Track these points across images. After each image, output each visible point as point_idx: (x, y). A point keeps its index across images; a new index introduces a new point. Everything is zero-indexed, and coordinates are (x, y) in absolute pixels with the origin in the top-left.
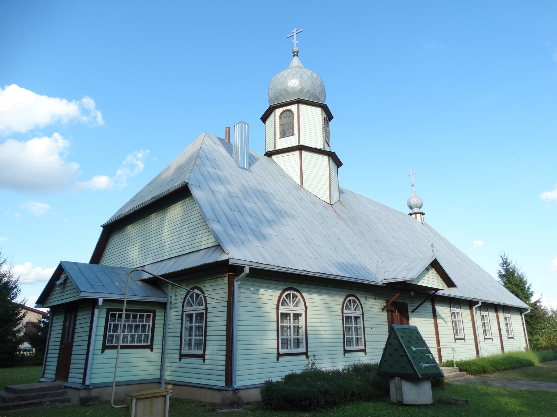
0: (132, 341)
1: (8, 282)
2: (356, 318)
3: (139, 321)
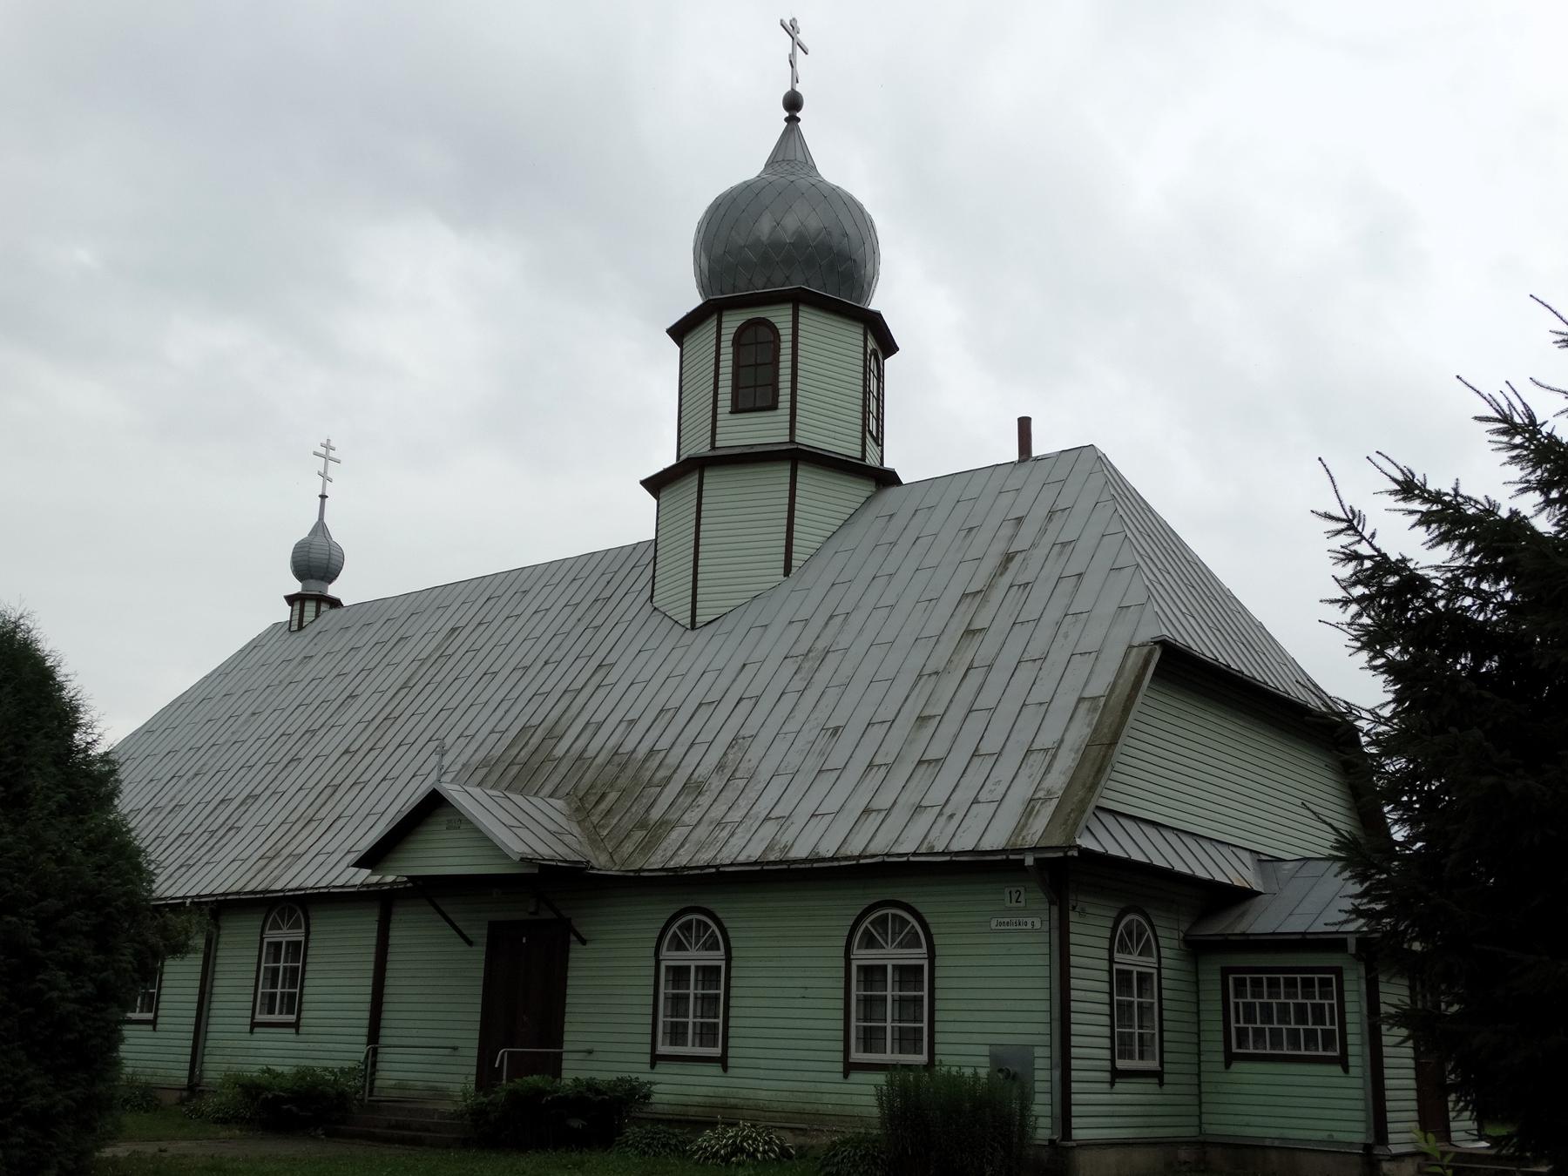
0: (1276, 1043)
2: (1144, 978)
3: (1270, 997)
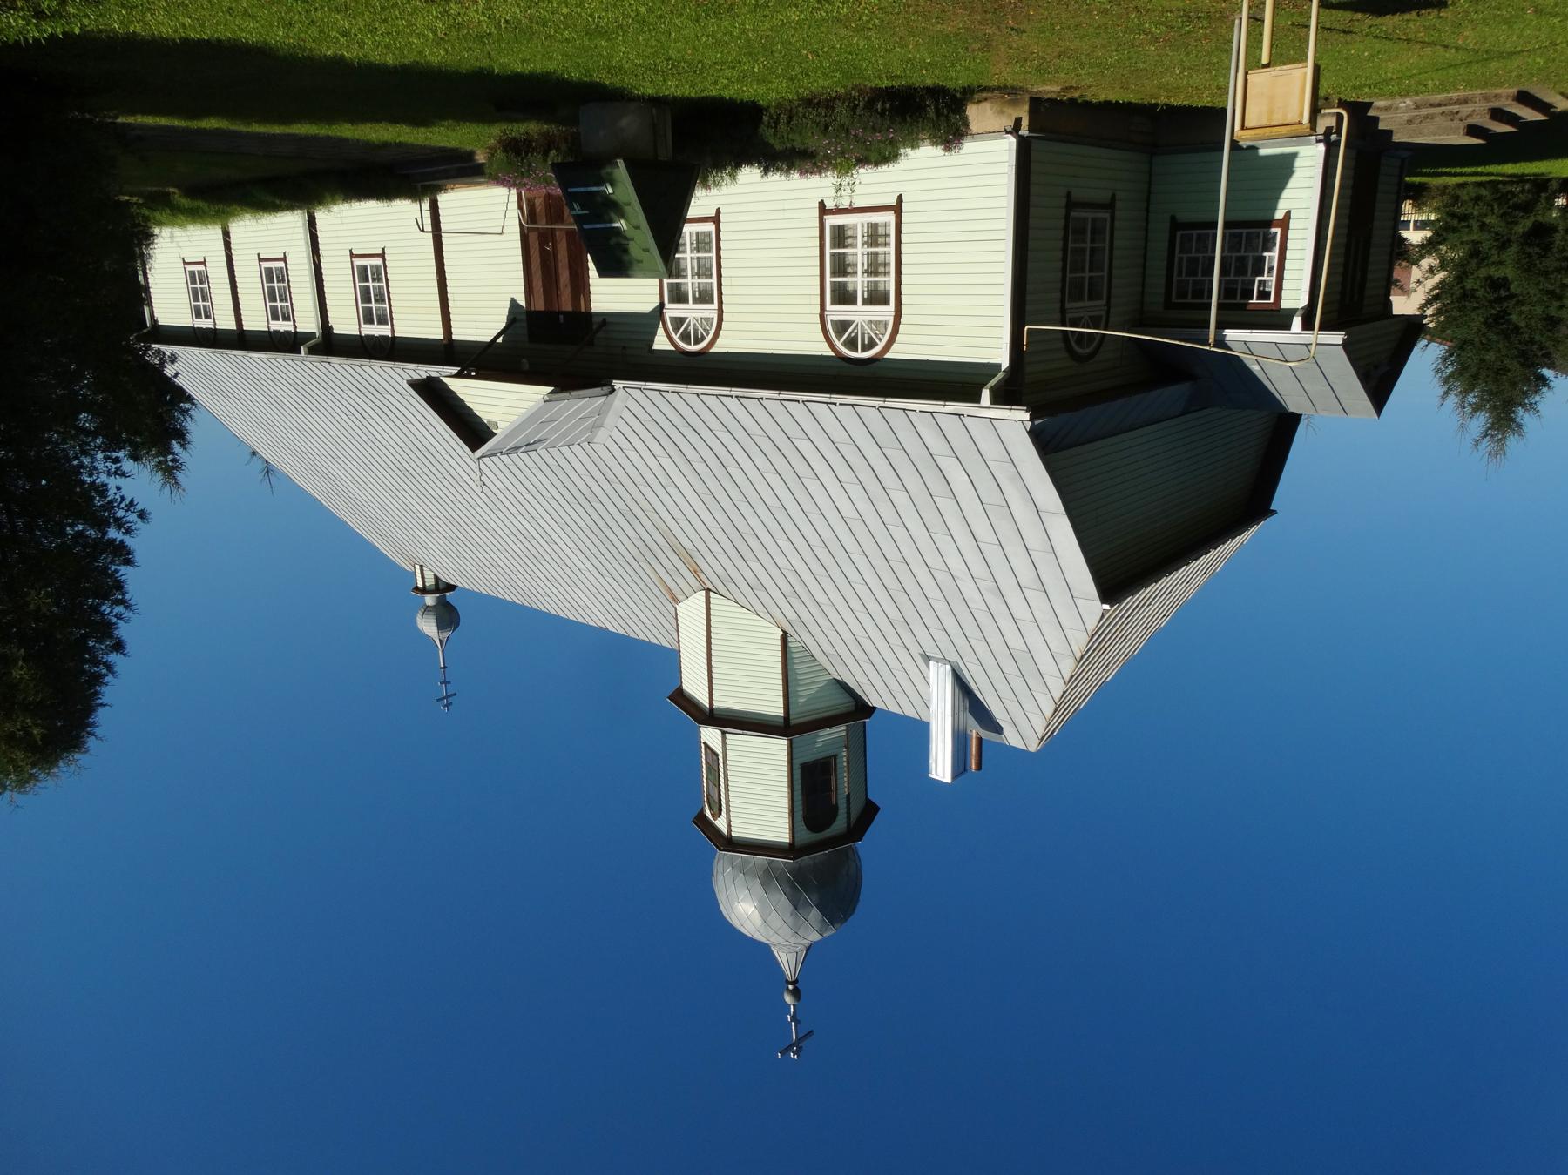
1: (1465, 392)
